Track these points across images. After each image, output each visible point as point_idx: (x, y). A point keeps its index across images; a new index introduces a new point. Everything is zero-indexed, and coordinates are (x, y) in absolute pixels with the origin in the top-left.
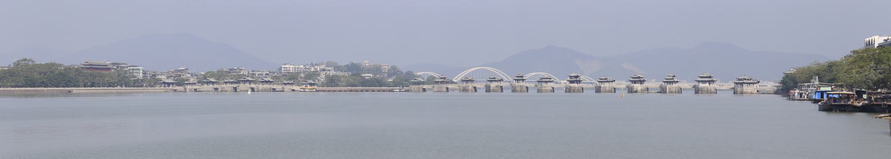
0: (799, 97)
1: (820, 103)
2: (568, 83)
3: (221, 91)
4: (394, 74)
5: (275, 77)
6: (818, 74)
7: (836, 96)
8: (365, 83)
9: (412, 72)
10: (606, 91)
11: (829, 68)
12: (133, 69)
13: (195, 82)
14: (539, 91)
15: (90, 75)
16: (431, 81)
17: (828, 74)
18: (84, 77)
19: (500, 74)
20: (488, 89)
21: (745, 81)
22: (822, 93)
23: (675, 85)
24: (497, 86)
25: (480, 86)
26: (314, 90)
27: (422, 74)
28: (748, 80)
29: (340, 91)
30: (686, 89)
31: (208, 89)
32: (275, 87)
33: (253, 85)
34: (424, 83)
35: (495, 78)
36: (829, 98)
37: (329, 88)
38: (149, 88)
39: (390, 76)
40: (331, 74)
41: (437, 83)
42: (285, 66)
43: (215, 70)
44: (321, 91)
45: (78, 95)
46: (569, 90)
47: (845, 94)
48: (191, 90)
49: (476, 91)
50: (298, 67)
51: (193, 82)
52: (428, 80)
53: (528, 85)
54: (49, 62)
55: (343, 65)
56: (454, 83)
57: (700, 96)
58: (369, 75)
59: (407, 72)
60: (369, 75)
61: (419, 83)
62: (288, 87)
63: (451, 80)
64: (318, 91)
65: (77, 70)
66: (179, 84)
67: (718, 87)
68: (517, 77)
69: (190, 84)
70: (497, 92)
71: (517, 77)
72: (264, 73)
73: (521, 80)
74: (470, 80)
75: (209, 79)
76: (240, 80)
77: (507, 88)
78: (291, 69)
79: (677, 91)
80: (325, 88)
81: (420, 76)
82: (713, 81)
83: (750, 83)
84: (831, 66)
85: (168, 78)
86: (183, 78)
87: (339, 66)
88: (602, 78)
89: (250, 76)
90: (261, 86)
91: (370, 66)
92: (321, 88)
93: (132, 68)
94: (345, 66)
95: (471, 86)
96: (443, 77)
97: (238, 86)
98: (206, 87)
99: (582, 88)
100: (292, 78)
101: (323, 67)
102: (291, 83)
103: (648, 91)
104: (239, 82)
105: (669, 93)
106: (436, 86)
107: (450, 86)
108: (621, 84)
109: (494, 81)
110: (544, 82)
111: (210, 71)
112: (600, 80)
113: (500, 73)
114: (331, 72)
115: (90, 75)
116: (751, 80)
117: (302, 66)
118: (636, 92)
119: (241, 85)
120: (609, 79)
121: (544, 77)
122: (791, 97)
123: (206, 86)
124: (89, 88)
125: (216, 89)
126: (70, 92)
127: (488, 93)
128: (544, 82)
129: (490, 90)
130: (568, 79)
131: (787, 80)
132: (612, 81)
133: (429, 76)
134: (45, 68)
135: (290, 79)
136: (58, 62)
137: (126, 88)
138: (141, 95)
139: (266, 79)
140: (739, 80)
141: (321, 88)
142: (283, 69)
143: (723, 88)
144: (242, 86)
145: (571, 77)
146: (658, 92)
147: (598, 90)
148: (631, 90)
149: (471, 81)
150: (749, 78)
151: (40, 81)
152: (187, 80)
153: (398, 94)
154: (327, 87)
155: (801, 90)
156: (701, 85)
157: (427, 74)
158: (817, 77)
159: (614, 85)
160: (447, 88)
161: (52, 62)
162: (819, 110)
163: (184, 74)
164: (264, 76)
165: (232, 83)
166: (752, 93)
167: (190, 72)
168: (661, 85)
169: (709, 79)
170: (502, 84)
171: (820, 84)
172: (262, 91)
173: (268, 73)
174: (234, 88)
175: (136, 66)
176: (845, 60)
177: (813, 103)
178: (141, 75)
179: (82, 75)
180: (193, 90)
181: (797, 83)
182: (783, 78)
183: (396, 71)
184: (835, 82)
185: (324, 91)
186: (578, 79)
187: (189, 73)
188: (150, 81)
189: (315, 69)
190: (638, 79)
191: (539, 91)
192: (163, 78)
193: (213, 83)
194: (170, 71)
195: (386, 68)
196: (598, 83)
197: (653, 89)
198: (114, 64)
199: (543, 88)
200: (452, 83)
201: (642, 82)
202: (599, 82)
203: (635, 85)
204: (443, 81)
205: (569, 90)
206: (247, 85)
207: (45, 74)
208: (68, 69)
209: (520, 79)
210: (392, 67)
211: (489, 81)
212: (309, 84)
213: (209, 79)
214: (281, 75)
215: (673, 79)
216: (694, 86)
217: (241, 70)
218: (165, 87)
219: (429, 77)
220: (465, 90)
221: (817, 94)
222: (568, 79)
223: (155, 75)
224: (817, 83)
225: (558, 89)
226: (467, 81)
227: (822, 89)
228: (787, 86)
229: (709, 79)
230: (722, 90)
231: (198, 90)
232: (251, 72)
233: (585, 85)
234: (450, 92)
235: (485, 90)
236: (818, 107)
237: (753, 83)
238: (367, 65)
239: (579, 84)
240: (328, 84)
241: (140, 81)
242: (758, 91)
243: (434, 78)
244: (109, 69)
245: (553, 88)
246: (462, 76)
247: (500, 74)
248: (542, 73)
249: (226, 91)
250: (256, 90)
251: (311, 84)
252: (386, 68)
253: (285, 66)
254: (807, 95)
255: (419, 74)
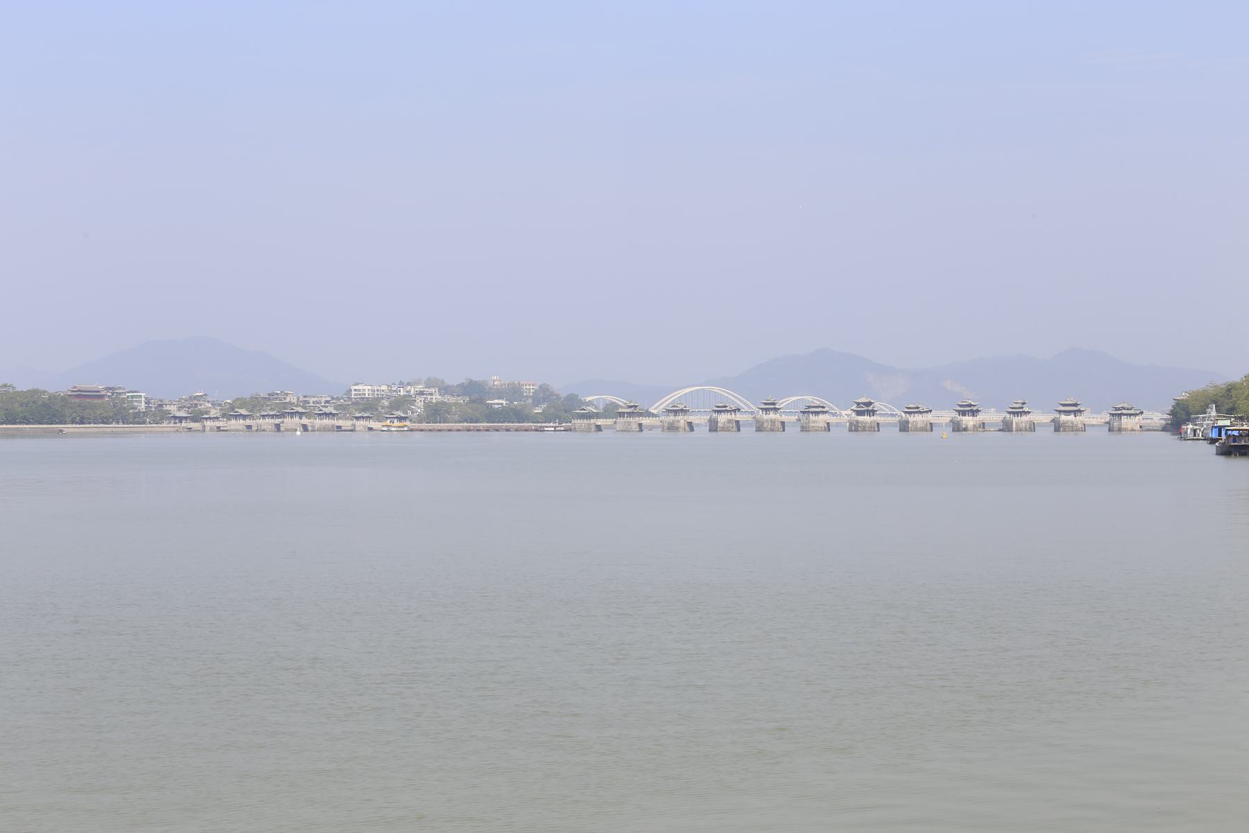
0: (1191, 436)
1: (1217, 444)
2: (854, 414)
3: (257, 431)
4: (544, 400)
5: (341, 405)
6: (1215, 402)
7: (1236, 433)
8: (494, 416)
9: (577, 396)
10: (916, 430)
11: (1228, 392)
12: (132, 397)
13: (218, 415)
14: (804, 429)
15: (79, 406)
16: (611, 411)
17: (1226, 401)
18: (71, 408)
19: (735, 400)
20: (713, 427)
21: (1124, 411)
22: (1220, 428)
23: (1025, 418)
24: (730, 421)
25: (700, 420)
26: (406, 429)
27: (595, 399)
28: (1128, 409)
29: (450, 430)
30: (1042, 425)
31: (236, 428)
32: (340, 423)
33: (305, 421)
34: (597, 416)
35: (726, 407)
36: (1228, 436)
37: (432, 426)
38: (154, 425)
39: (537, 402)
40: (434, 401)
41: (622, 415)
42: (356, 387)
43: (247, 396)
44: (417, 430)
45: (72, 435)
46: (855, 427)
47: (1247, 430)
48: (212, 429)
49: (692, 429)
50: (379, 388)
51: (215, 416)
52: (606, 409)
53: (784, 418)
54: (31, 388)
55: (455, 385)
56: (654, 415)
57: (1062, 435)
58: (500, 401)
59: (568, 396)
60: (500, 401)
61: (589, 416)
62: (362, 422)
63: (647, 411)
64: (411, 430)
65: (63, 399)
66: (195, 420)
67: (1087, 421)
68: (766, 404)
69: (210, 418)
70: (729, 431)
71: (766, 404)
72: (323, 400)
73: (772, 409)
74: (682, 410)
75: (239, 410)
76: (284, 411)
77: (748, 424)
78: (367, 392)
79: (1028, 427)
80: (424, 424)
81: (590, 404)
82: (1080, 411)
83: (1131, 415)
84: (1230, 389)
85: (180, 409)
86: (200, 409)
87: (448, 387)
88: (911, 406)
89: (300, 406)
90: (318, 422)
91: (501, 385)
92: (416, 425)
93: (131, 394)
94: (458, 385)
95: (682, 421)
96: (632, 404)
97: (283, 422)
98: (234, 424)
99: (878, 424)
100: (369, 407)
101: (420, 388)
102: (367, 417)
103: (984, 428)
104: (283, 415)
105: (1017, 431)
106: (620, 420)
107: (645, 421)
108: (943, 417)
109: (916, 412)
110: (812, 412)
111: (240, 397)
112: (1010, 410)
113: (736, 398)
114: (434, 397)
115: (79, 406)
116: (1131, 409)
117: (384, 388)
118: (965, 429)
119: (285, 420)
120: (923, 408)
121: (812, 405)
122: (1183, 436)
123: (233, 421)
124: (78, 426)
125: (249, 427)
126: (61, 431)
127: (714, 434)
128: (812, 412)
129: (717, 428)
130: (854, 407)
131: (1178, 409)
132: (927, 412)
133: (608, 402)
134: (26, 398)
135: (364, 410)
136: (42, 388)
137: (123, 426)
138: (143, 435)
139: (327, 410)
140: (1117, 409)
141: (416, 425)
142: (353, 392)
143: (1095, 423)
144: (288, 422)
145: (858, 404)
146: (1000, 430)
147: (904, 427)
148: (957, 427)
149: (684, 411)
150: (1129, 407)
151: (21, 415)
152: (207, 413)
153: (552, 436)
154: (428, 423)
155: (1195, 425)
156: (1063, 418)
157: (604, 400)
158: (1214, 405)
159: (929, 418)
160: (640, 425)
161: (35, 388)
162: (1217, 454)
163: (202, 402)
164: (323, 404)
165: (273, 416)
166: (1133, 430)
167: (210, 399)
168: (1005, 418)
169: (1074, 408)
170: (738, 417)
171: (1218, 416)
172: (319, 430)
173: (329, 399)
174: (276, 425)
175: (136, 392)
176: (1246, 381)
177: (1210, 443)
178: (143, 406)
179: (69, 406)
180: (215, 429)
181: (1191, 414)
182: (1173, 407)
183: (547, 393)
184: (1235, 412)
185: (421, 430)
186: (870, 408)
187: (209, 402)
188: (154, 415)
189: (407, 392)
190: (969, 409)
191: (804, 429)
192: (173, 409)
193: (244, 417)
194: (183, 399)
195: (530, 389)
196: (903, 415)
197: (992, 424)
198: (108, 389)
199: (811, 425)
200: (650, 415)
201: (974, 413)
202: (906, 412)
203: (964, 418)
204: (633, 412)
205: (855, 427)
206: (296, 419)
207: (27, 406)
208: (53, 397)
209: (771, 407)
210: (540, 387)
211: (715, 411)
212: (397, 417)
213: (239, 410)
214: (350, 403)
215: (1022, 408)
216: (1053, 421)
217: (287, 394)
218: (175, 423)
219: (607, 405)
220: (672, 428)
221: (1214, 430)
222: (854, 407)
223: (161, 406)
224: (1214, 413)
225: (838, 425)
226: (676, 412)
227: (1220, 423)
228: (1179, 419)
229: (1074, 408)
230: (1093, 425)
231: (222, 428)
232: (301, 399)
233: (883, 419)
234: (645, 431)
235: (708, 428)
236: (1215, 447)
237: (1135, 415)
238: (496, 383)
239: (872, 418)
240: (428, 418)
241: (142, 415)
242: (1141, 427)
243: (617, 406)
244: (102, 397)
245: (828, 424)
246: (667, 402)
247: (735, 400)
248: (810, 398)
249: (264, 430)
250: (310, 428)
251: (400, 419)
252: (530, 389)
253: (356, 387)
254: (1202, 433)
255: (588, 399)
